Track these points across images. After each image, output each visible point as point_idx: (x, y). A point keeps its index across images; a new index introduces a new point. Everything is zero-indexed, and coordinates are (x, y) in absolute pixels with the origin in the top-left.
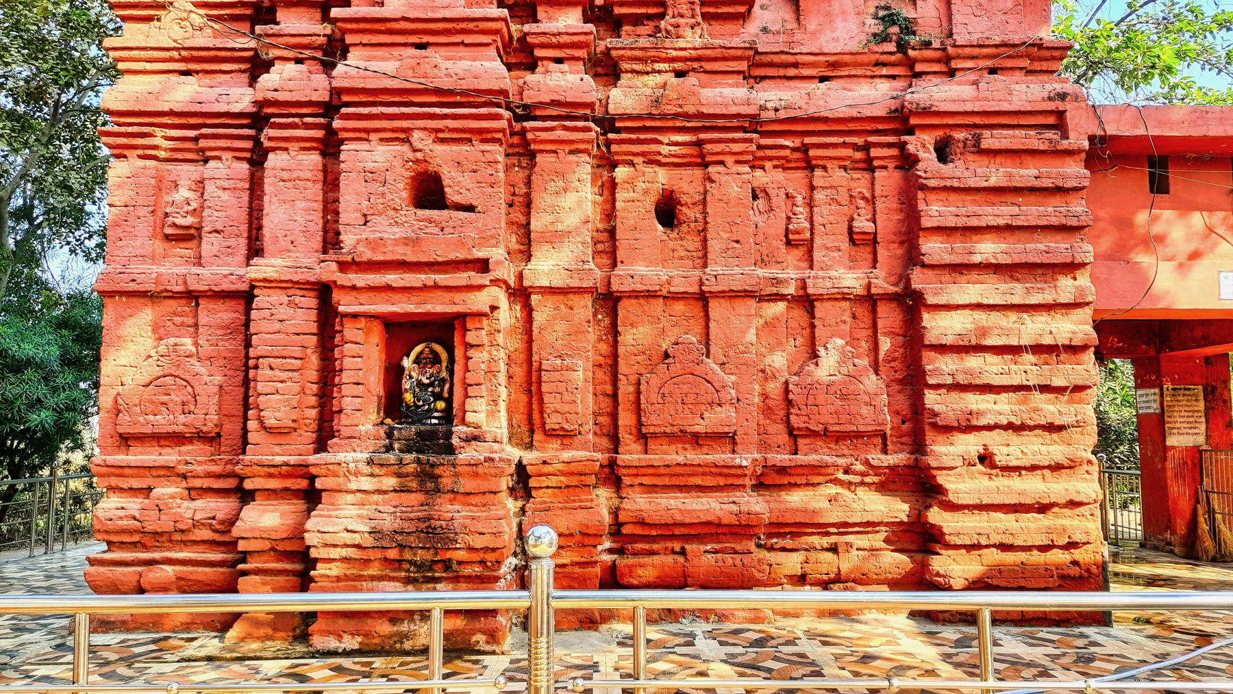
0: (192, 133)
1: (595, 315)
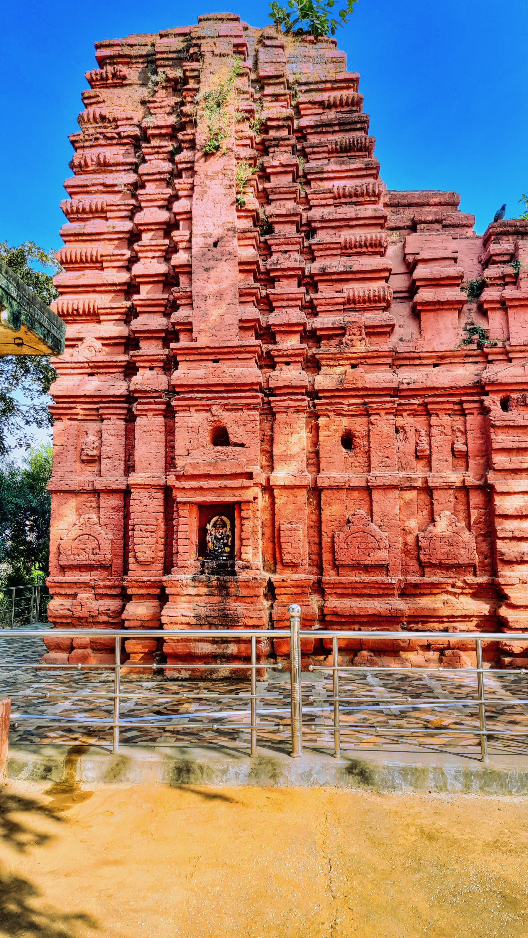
0: (96, 406)
1: (308, 499)
